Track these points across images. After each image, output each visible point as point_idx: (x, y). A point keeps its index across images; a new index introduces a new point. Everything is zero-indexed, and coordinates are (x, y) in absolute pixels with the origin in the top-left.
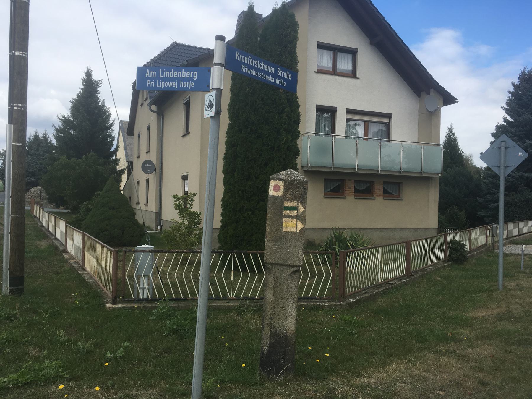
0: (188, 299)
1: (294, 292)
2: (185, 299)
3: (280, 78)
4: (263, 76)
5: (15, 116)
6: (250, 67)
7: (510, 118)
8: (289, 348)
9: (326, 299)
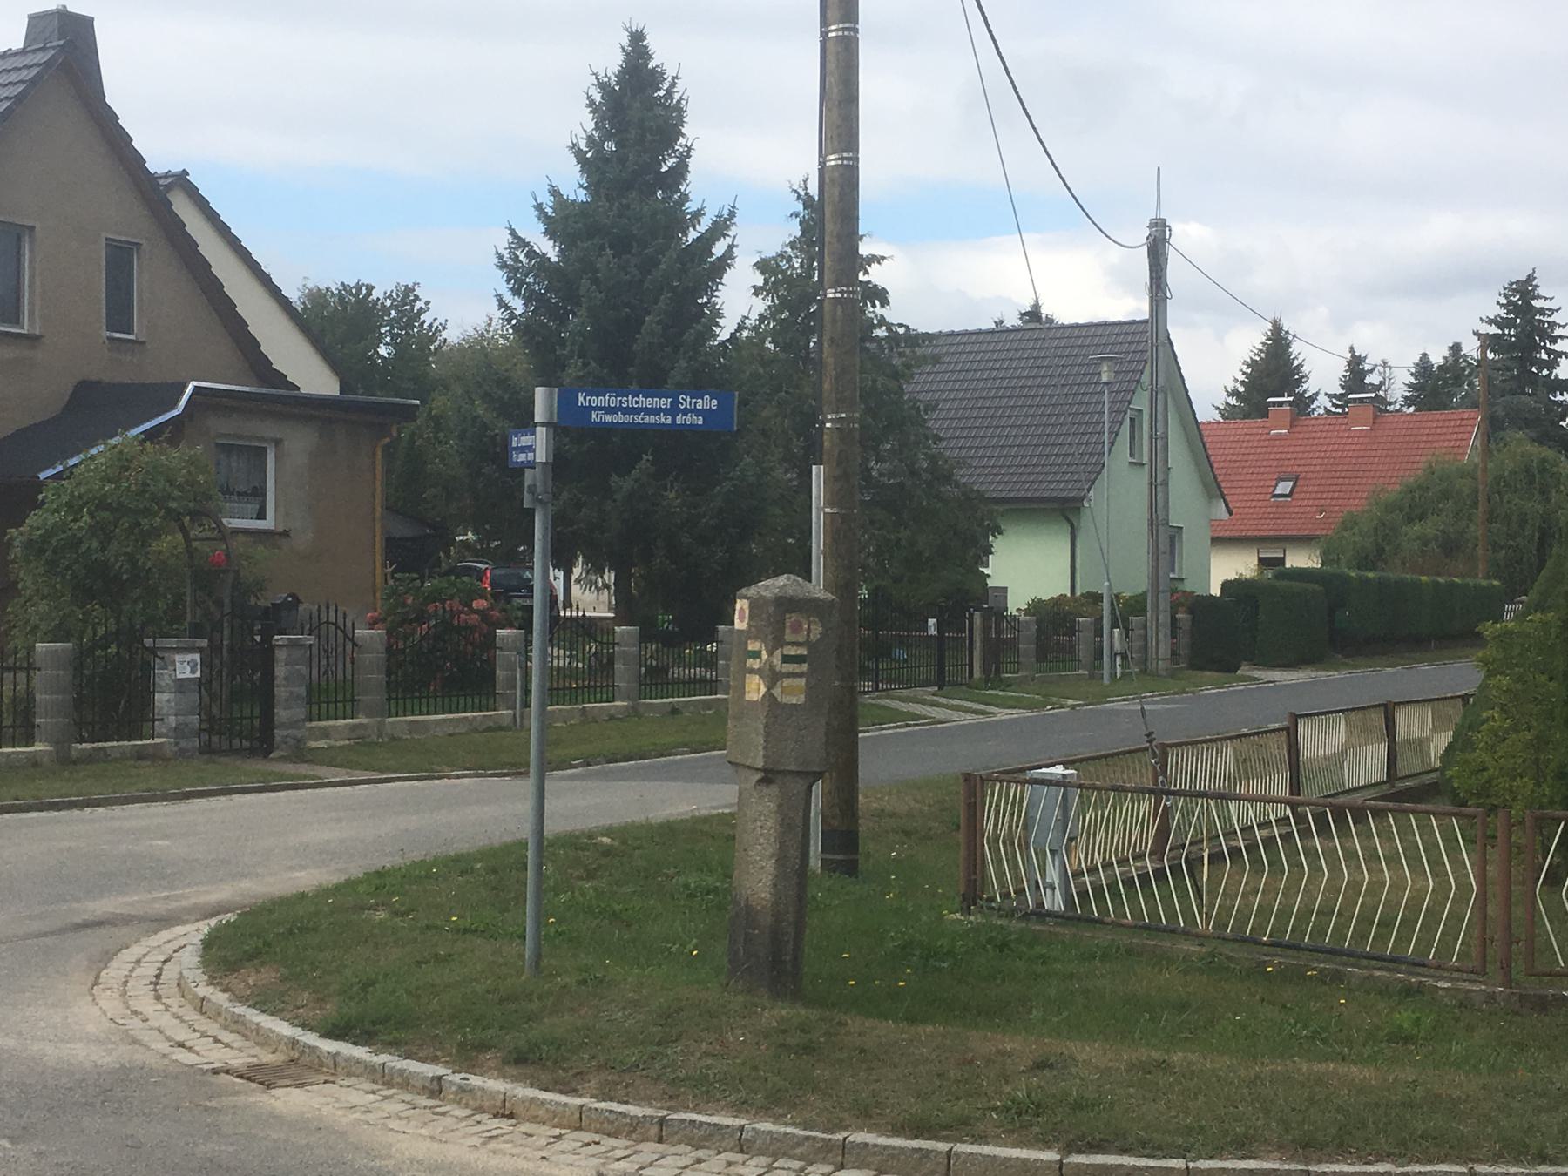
0: (1107, 919)
3: (685, 412)
4: (643, 419)
6: (609, 410)
7: (1410, 385)
9: (1458, 970)
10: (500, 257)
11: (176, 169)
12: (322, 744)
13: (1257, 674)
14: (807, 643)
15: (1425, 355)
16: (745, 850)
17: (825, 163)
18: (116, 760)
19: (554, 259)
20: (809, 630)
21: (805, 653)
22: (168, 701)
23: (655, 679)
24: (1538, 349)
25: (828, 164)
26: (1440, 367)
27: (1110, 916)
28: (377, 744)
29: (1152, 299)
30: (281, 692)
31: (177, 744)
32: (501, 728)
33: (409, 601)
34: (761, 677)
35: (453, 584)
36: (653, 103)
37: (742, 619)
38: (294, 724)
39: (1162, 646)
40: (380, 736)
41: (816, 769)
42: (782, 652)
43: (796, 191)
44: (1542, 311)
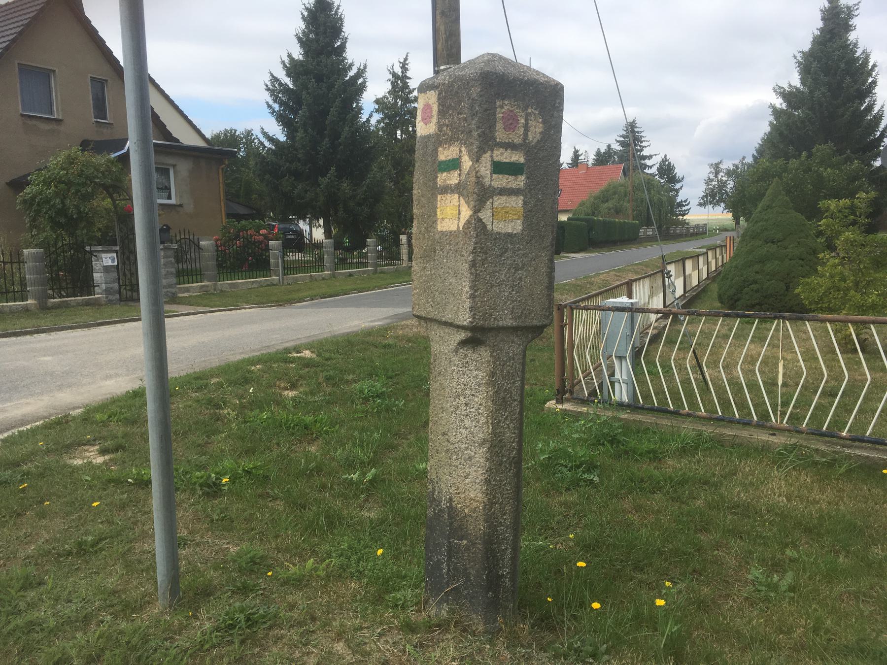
0: (681, 411)
1: (476, 399)
2: (676, 413)
7: (594, 159)
8: (465, 542)
10: (267, 85)
12: (186, 295)
13: (567, 255)
15: (599, 149)
18: (73, 306)
19: (291, 86)
20: (527, 128)
21: (522, 160)
22: (101, 276)
23: (342, 262)
27: (684, 408)
28: (213, 294)
31: (107, 297)
32: (274, 285)
34: (461, 194)
35: (251, 223)
36: (329, 16)
37: (426, 120)
38: (170, 286)
40: (215, 290)
41: (536, 322)
42: (492, 156)
43: (389, 70)
44: (638, 132)
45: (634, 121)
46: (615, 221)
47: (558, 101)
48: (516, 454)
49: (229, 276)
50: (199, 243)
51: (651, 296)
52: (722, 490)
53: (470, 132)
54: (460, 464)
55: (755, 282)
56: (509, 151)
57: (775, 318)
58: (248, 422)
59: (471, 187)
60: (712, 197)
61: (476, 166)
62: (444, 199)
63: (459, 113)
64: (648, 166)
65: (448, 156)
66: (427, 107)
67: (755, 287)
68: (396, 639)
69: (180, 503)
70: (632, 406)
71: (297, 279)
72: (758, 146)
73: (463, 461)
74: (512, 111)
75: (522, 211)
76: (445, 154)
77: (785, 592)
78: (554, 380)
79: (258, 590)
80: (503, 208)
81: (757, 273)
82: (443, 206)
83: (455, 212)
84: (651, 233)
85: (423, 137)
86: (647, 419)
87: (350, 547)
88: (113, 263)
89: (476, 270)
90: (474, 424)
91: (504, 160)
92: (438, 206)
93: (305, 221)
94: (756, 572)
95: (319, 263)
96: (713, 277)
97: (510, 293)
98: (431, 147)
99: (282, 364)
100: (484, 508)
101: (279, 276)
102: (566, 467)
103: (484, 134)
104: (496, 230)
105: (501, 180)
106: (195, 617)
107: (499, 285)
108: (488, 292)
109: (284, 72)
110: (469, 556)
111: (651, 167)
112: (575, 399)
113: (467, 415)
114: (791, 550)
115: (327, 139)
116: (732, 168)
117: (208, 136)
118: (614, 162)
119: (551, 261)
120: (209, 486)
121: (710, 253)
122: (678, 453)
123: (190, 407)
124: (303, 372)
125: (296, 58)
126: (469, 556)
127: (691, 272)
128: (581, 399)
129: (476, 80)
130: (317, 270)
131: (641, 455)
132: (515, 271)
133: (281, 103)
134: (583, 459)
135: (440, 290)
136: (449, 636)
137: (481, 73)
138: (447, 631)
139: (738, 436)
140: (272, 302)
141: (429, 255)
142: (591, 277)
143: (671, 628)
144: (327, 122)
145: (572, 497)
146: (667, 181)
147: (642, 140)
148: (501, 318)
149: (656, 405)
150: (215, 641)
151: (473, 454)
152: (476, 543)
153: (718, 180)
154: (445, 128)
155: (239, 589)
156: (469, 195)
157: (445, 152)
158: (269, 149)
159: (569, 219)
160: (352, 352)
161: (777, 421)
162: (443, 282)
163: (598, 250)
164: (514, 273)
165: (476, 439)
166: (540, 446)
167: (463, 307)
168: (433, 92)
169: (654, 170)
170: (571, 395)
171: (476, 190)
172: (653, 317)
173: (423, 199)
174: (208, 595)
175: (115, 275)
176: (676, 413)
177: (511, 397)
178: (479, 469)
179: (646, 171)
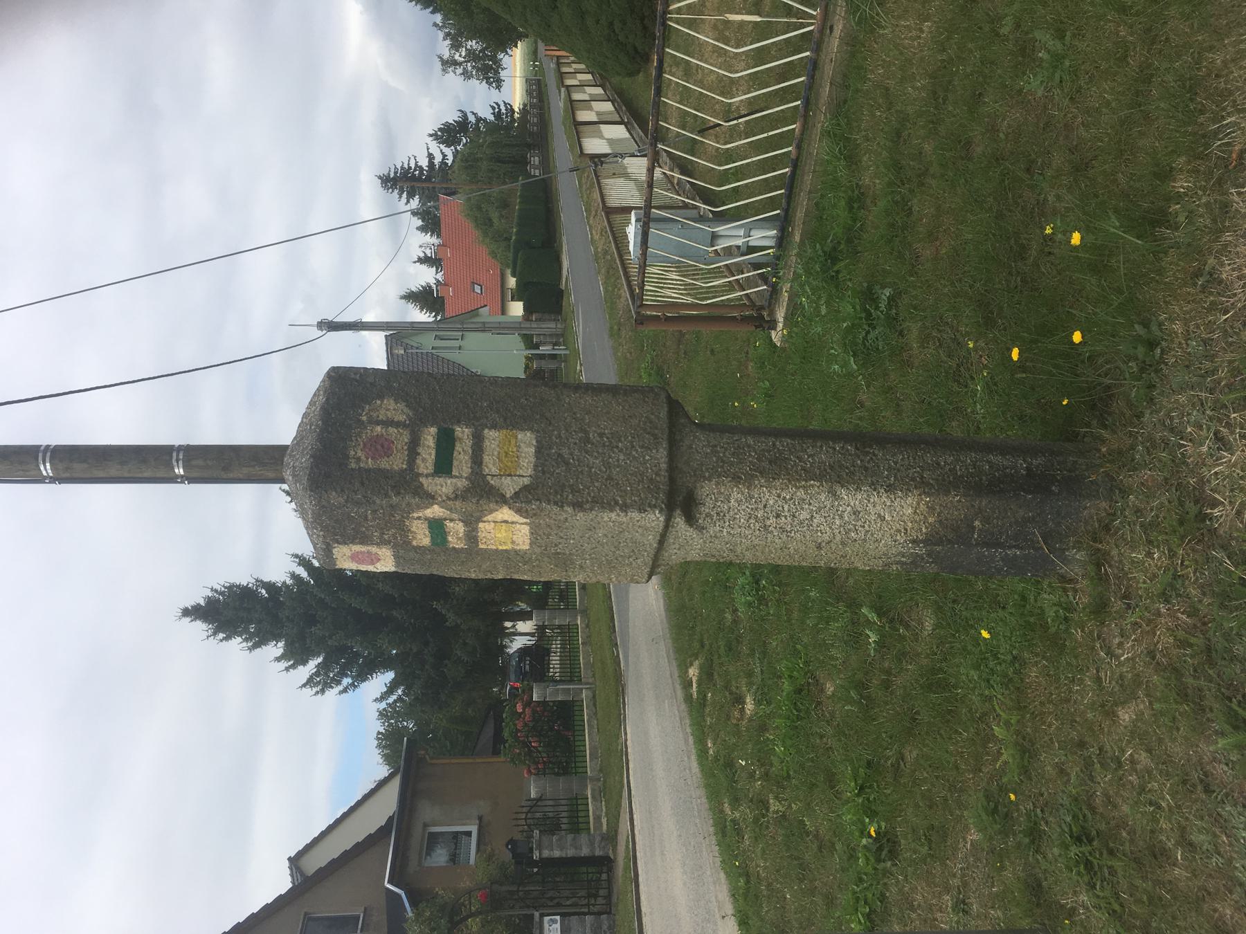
0: (793, 156)
1: (771, 502)
2: (795, 165)
5: (195, 474)
7: (431, 236)
10: (317, 693)
11: (287, 864)
12: (604, 821)
13: (564, 280)
14: (415, 429)
15: (417, 228)
16: (819, 547)
17: (51, 478)
19: (320, 660)
20: (389, 423)
21: (433, 430)
24: (414, 175)
25: (51, 475)
26: (423, 221)
28: (605, 782)
29: (361, 330)
30: (571, 853)
32: (594, 697)
33: (518, 751)
34: (479, 520)
36: (226, 604)
37: (375, 559)
38: (592, 844)
39: (549, 326)
41: (663, 413)
42: (427, 476)
44: (396, 173)
45: (380, 177)
46: (520, 210)
47: (353, 376)
48: (851, 445)
49: (580, 759)
50: (534, 800)
51: (626, 176)
52: (910, 110)
53: (391, 506)
54: (864, 527)
55: (611, 24)
56: (420, 450)
57: (664, 24)
58: (788, 772)
59: (470, 506)
60: (490, 72)
61: (440, 499)
62: (485, 540)
63: (366, 519)
64: (443, 160)
65: (425, 534)
66: (354, 557)
67: (617, 25)
68: (1117, 632)
69: (903, 894)
70: (784, 225)
71: (587, 663)
72: (419, 7)
73: (859, 523)
74: (365, 445)
75: (505, 431)
76: (422, 537)
77: (1064, 45)
78: (743, 331)
79: (1036, 815)
80: (500, 460)
81: (597, 22)
82: (495, 541)
83: (504, 527)
84: (537, 159)
85: (397, 564)
86: (802, 204)
87: (977, 667)
88: (557, 921)
89: (587, 502)
90: (807, 506)
91: (433, 457)
92: (495, 548)
93: (506, 647)
94: (1034, 84)
95: (567, 632)
96: (601, 80)
97: (621, 451)
98: (412, 554)
99: (707, 710)
100: (928, 495)
101: (582, 689)
102: (868, 332)
103: (395, 486)
104: (530, 472)
105: (461, 462)
106: (1071, 913)
107: (610, 467)
108: (618, 484)
109: (301, 667)
110: (998, 518)
111: (444, 156)
112: (770, 304)
113: (794, 516)
114: (1002, 26)
115: (394, 613)
116: (448, 42)
117: (383, 771)
118: (437, 208)
119: (580, 388)
120: (880, 849)
121: (569, 82)
122: (854, 167)
123: (764, 851)
124: (720, 683)
125: (281, 651)
126: (998, 518)
127: (594, 113)
128: (771, 296)
129: (321, 497)
130: (575, 634)
131: (855, 220)
132: (589, 443)
133: (343, 674)
134: (858, 307)
135: (613, 549)
136: (1114, 552)
137: (311, 491)
138: (1107, 554)
139: (832, 79)
140: (617, 701)
141: (564, 561)
142: (596, 253)
143: (1113, 225)
144: (370, 612)
145: (914, 330)
146: (465, 134)
147: (407, 167)
148: (656, 466)
149: (783, 191)
150: (1107, 893)
151: (849, 508)
152: (979, 508)
153: (466, 62)
154: (386, 537)
155: (1033, 842)
156: (480, 509)
157: (419, 537)
158: (404, 693)
159: (514, 275)
160: (693, 609)
161: (812, 24)
162: (602, 545)
163: (557, 235)
164: (593, 444)
165: (828, 504)
166: (836, 367)
167: (638, 521)
168: (335, 551)
169: (449, 152)
170: (764, 309)
171: (474, 501)
172: (658, 173)
173: (484, 566)
174: (1040, 885)
175: (574, 919)
176: (795, 165)
177: (769, 451)
178: (872, 500)
179: (449, 162)
